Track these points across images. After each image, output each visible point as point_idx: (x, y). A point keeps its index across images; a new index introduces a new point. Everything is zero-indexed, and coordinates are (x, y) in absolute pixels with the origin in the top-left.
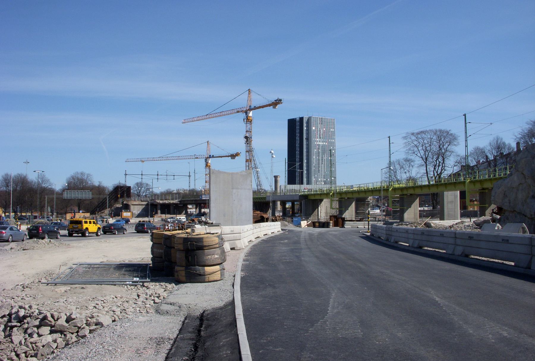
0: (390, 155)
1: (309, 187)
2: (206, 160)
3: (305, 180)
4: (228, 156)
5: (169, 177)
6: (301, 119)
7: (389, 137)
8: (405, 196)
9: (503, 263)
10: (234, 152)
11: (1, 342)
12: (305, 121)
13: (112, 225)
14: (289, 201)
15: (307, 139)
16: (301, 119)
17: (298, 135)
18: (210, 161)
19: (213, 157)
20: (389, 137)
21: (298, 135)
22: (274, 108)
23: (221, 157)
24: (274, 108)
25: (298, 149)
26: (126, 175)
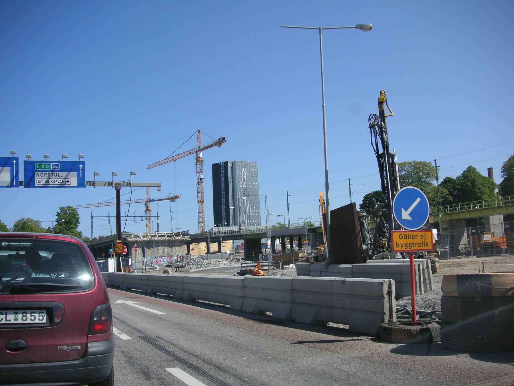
0: (350, 194)
1: (236, 228)
2: (146, 205)
3: (232, 222)
4: (168, 199)
5: (137, 219)
6: (226, 163)
7: (349, 179)
8: (454, 222)
9: (343, 282)
10: (173, 195)
11: (493, 325)
12: (230, 165)
13: (483, 233)
14: (296, 236)
15: (233, 182)
16: (226, 163)
17: (223, 179)
18: (150, 204)
19: (153, 200)
20: (349, 179)
21: (223, 179)
22: (219, 146)
23: (161, 200)
24: (219, 146)
25: (223, 192)
26: (92, 217)
